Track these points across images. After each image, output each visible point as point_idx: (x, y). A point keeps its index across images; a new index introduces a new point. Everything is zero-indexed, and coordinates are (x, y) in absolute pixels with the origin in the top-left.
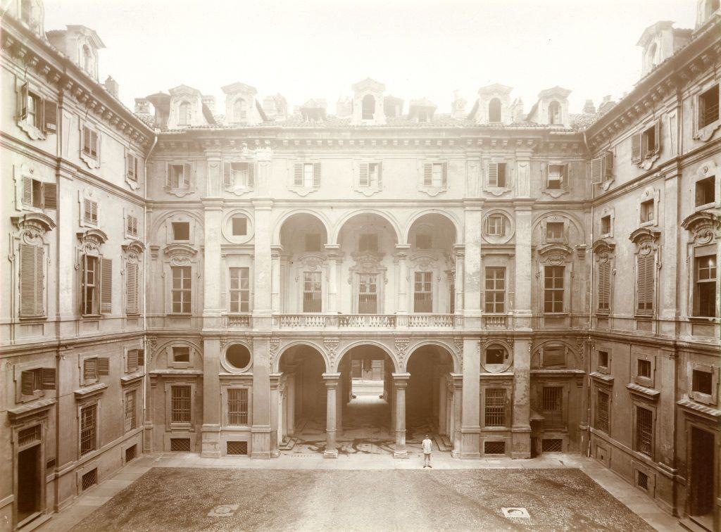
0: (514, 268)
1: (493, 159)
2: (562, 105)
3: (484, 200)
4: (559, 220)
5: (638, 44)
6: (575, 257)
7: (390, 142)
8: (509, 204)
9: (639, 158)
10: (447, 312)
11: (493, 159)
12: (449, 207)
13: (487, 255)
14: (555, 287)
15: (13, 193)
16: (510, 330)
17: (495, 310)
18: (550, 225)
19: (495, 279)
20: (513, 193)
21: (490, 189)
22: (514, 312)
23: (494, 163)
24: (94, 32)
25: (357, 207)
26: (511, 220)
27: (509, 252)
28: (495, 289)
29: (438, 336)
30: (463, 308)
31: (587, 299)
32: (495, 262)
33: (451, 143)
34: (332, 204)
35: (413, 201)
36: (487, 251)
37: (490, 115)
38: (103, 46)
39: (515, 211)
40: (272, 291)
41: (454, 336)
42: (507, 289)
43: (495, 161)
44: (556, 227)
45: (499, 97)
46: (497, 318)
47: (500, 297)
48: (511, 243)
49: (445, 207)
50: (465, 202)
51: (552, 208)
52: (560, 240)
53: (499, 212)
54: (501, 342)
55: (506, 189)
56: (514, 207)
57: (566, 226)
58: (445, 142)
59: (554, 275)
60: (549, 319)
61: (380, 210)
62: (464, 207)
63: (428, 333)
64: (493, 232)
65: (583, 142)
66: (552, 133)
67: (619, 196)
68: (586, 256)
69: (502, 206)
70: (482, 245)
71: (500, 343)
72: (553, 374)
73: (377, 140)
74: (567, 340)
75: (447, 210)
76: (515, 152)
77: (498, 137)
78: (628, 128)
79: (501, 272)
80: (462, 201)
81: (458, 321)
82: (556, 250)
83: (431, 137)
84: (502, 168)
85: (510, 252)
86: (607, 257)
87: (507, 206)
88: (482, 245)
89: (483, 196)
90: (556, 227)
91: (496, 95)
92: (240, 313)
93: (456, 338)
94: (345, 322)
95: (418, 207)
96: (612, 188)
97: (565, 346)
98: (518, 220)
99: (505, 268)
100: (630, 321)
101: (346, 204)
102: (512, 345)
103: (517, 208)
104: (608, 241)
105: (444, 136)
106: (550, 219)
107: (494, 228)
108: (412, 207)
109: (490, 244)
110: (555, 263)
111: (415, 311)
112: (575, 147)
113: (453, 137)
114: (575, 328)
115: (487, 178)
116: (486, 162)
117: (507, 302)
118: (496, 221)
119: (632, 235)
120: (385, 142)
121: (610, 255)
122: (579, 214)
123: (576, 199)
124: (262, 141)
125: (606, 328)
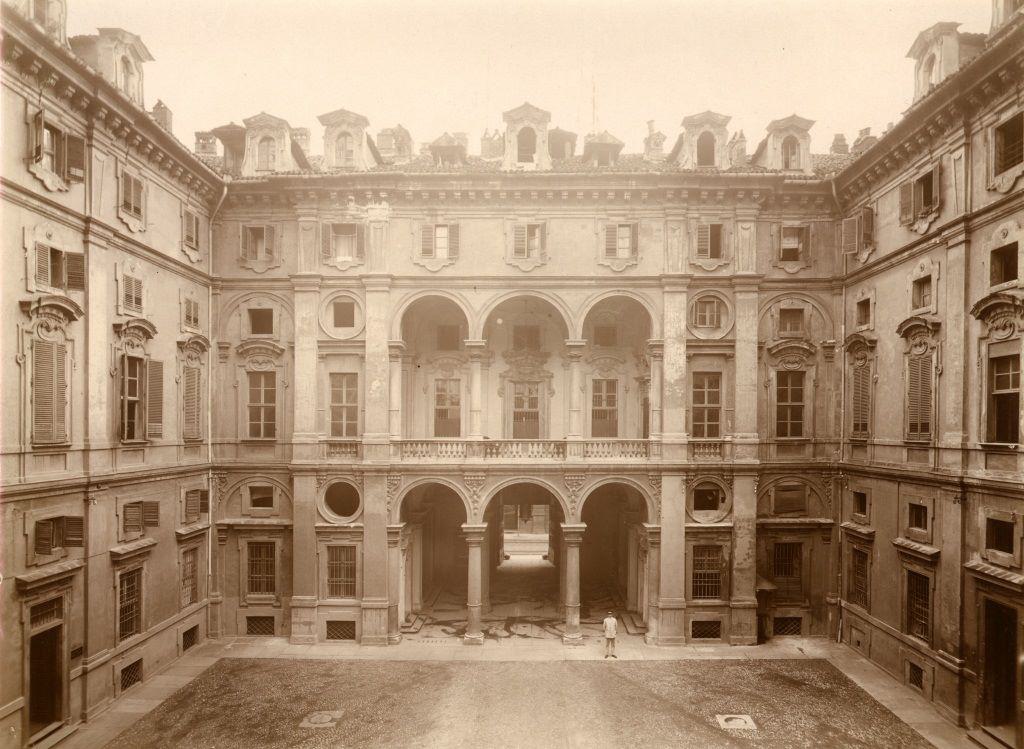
0: (734, 373)
1: (703, 219)
4: (798, 305)
6: (819, 358)
9: (911, 216)
11: (703, 219)
12: (641, 286)
16: (728, 461)
17: (344, 434)
18: (784, 312)
21: (700, 262)
22: (733, 437)
23: (705, 223)
25: (509, 287)
27: (726, 351)
34: (477, 283)
36: (695, 350)
39: (734, 293)
41: (647, 470)
44: (791, 316)
47: (714, 415)
48: (729, 337)
49: (635, 286)
51: (787, 288)
52: (799, 333)
53: (712, 294)
54: (715, 479)
55: (722, 262)
56: (732, 286)
57: (807, 313)
58: (636, 194)
60: (782, 447)
61: (450, 291)
66: (787, 181)
69: (717, 285)
70: (688, 341)
71: (714, 481)
74: (809, 477)
75: (454, 292)
76: (735, 209)
77: (710, 188)
79: (715, 379)
80: (659, 278)
81: (655, 449)
82: (792, 348)
84: (716, 232)
85: (728, 352)
86: (865, 358)
87: (723, 286)
88: (688, 341)
90: (791, 316)
91: (707, 128)
102: (731, 483)
104: (866, 335)
105: (633, 185)
106: (785, 304)
107: (705, 317)
114: (819, 459)
117: (724, 422)
118: (708, 307)
119: (901, 327)
121: (870, 355)
122: (826, 297)
125: (862, 459)
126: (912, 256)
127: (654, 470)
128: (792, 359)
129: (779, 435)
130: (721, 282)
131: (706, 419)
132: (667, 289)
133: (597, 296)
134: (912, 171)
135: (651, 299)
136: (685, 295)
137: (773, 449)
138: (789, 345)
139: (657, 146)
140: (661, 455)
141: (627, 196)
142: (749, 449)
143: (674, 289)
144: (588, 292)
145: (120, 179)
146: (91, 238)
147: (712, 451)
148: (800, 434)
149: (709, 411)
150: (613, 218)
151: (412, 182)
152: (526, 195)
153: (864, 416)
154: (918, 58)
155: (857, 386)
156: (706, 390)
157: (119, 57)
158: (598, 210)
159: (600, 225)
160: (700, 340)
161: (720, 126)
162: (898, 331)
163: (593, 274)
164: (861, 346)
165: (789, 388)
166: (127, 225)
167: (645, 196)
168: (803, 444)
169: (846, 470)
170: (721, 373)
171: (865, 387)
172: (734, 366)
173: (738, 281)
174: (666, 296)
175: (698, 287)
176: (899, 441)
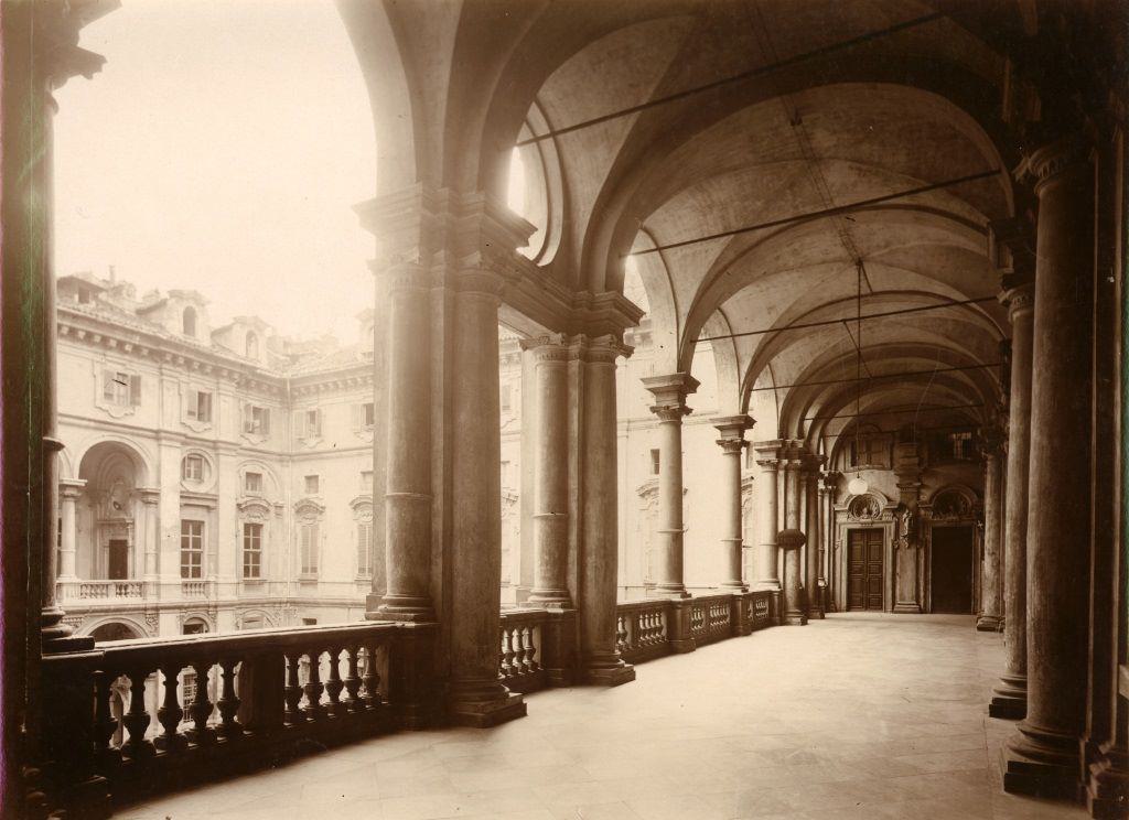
0: (217, 524)
2: (199, 314)
3: (185, 435)
7: (105, 340)
8: (211, 445)
10: (94, 577)
12: (138, 435)
14: (193, 547)
16: (212, 599)
17: (190, 576)
18: (249, 475)
24: (256, 317)
27: (209, 504)
28: (191, 549)
32: (195, 515)
36: (188, 500)
37: (64, 279)
38: (209, 302)
41: (145, 609)
43: (196, 388)
45: (194, 306)
46: (92, 586)
48: (213, 492)
49: (132, 434)
50: (163, 435)
51: (251, 456)
53: (199, 452)
55: (208, 425)
58: (137, 349)
63: (112, 607)
64: (189, 477)
66: (258, 371)
67: (332, 458)
69: (203, 445)
70: (181, 492)
72: (1014, 555)
75: (136, 439)
76: (161, 368)
77: (202, 360)
80: (157, 432)
81: (151, 590)
83: (118, 337)
84: (203, 399)
86: (315, 518)
87: (208, 447)
88: (181, 492)
89: (183, 431)
91: (191, 304)
92: (190, 580)
97: (263, 616)
98: (222, 466)
101: (92, 424)
102: (214, 618)
103: (221, 451)
105: (137, 340)
106: (250, 469)
107: (189, 471)
108: (87, 427)
109: (188, 492)
110: (254, 520)
111: (110, 578)
114: (273, 595)
117: (205, 565)
118: (193, 463)
119: (353, 502)
121: (319, 517)
122: (277, 467)
123: (273, 449)
125: (309, 593)
126: (360, 455)
127: (152, 609)
130: (207, 443)
132: (164, 442)
135: (145, 448)
136: (178, 450)
137: (242, 586)
138: (255, 502)
144: (88, 433)
146: (164, 371)
147: (202, 590)
148: (199, 576)
149: (194, 555)
151: (263, 364)
152: (89, 337)
161: (203, 305)
162: (351, 504)
165: (251, 537)
167: (145, 352)
170: (203, 522)
171: (314, 540)
174: (163, 449)
175: (187, 444)
176: (350, 580)
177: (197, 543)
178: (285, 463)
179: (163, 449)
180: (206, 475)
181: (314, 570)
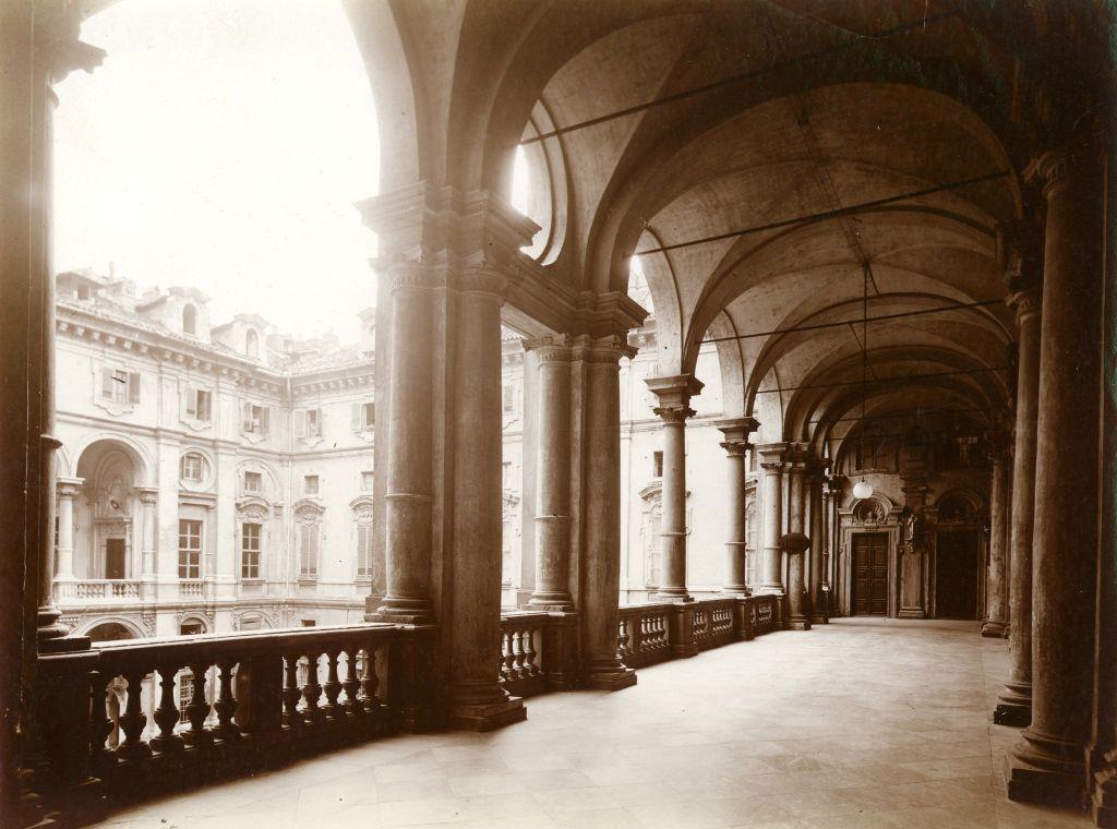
1: (191, 383)
2: (199, 311)
5: (358, 315)
8: (210, 443)
9: (359, 427)
11: (191, 383)
12: (136, 433)
13: (184, 504)
15: (67, 411)
16: (210, 600)
18: (248, 474)
19: (189, 536)
20: (213, 430)
21: (187, 421)
23: (193, 387)
26: (211, 463)
27: (208, 503)
29: (121, 610)
30: (215, 573)
31: (284, 563)
32: (193, 514)
33: (144, 350)
35: (88, 418)
36: (186, 499)
39: (158, 444)
40: (143, 549)
41: (143, 609)
42: (204, 549)
43: (196, 386)
44: (252, 477)
45: (195, 304)
47: (195, 558)
48: (212, 492)
49: (131, 433)
52: (256, 493)
53: (198, 451)
55: (207, 424)
58: (136, 347)
59: (189, 532)
60: (246, 585)
62: (281, 461)
64: (188, 476)
65: (286, 388)
66: (259, 370)
68: (284, 515)
71: (198, 616)
73: (201, 361)
74: (264, 610)
75: (134, 437)
78: (762, 530)
79: (196, 526)
80: (155, 430)
81: (148, 589)
83: (118, 335)
85: (210, 503)
87: (207, 446)
88: (180, 491)
90: (252, 477)
93: (146, 612)
94: (120, 591)
95: (94, 426)
96: (317, 449)
99: (201, 522)
100: (347, 587)
102: (212, 618)
105: (136, 338)
106: (250, 468)
112: (275, 389)
113: (148, 343)
115: (184, 406)
116: (183, 384)
117: (203, 565)
118: (191, 462)
119: (353, 502)
120: (80, 331)
121: (318, 518)
122: (276, 466)
123: (274, 449)
124: (231, 371)
125: (307, 595)
128: (255, 514)
129: (243, 576)
131: (188, 560)
133: (94, 436)
134: (361, 396)
137: (240, 587)
139: (129, 293)
140: (156, 594)
141: (127, 345)
142: (228, 588)
143: (169, 442)
145: (183, 395)
147: (195, 590)
149: (191, 555)
150: (109, 361)
152: (88, 333)
153: (314, 558)
154: (364, 320)
155: (304, 541)
156: (189, 536)
157: (181, 307)
158: (94, 350)
159: (96, 365)
160: (187, 491)
161: (203, 303)
162: (351, 505)
163: (88, 414)
164: (307, 510)
166: (189, 426)
167: (144, 350)
168: (260, 583)
169: (293, 604)
170: (201, 522)
172: (216, 517)
173: (222, 444)
177: (195, 543)
178: (285, 463)
179: (162, 447)
180: (205, 474)
181: (313, 571)
